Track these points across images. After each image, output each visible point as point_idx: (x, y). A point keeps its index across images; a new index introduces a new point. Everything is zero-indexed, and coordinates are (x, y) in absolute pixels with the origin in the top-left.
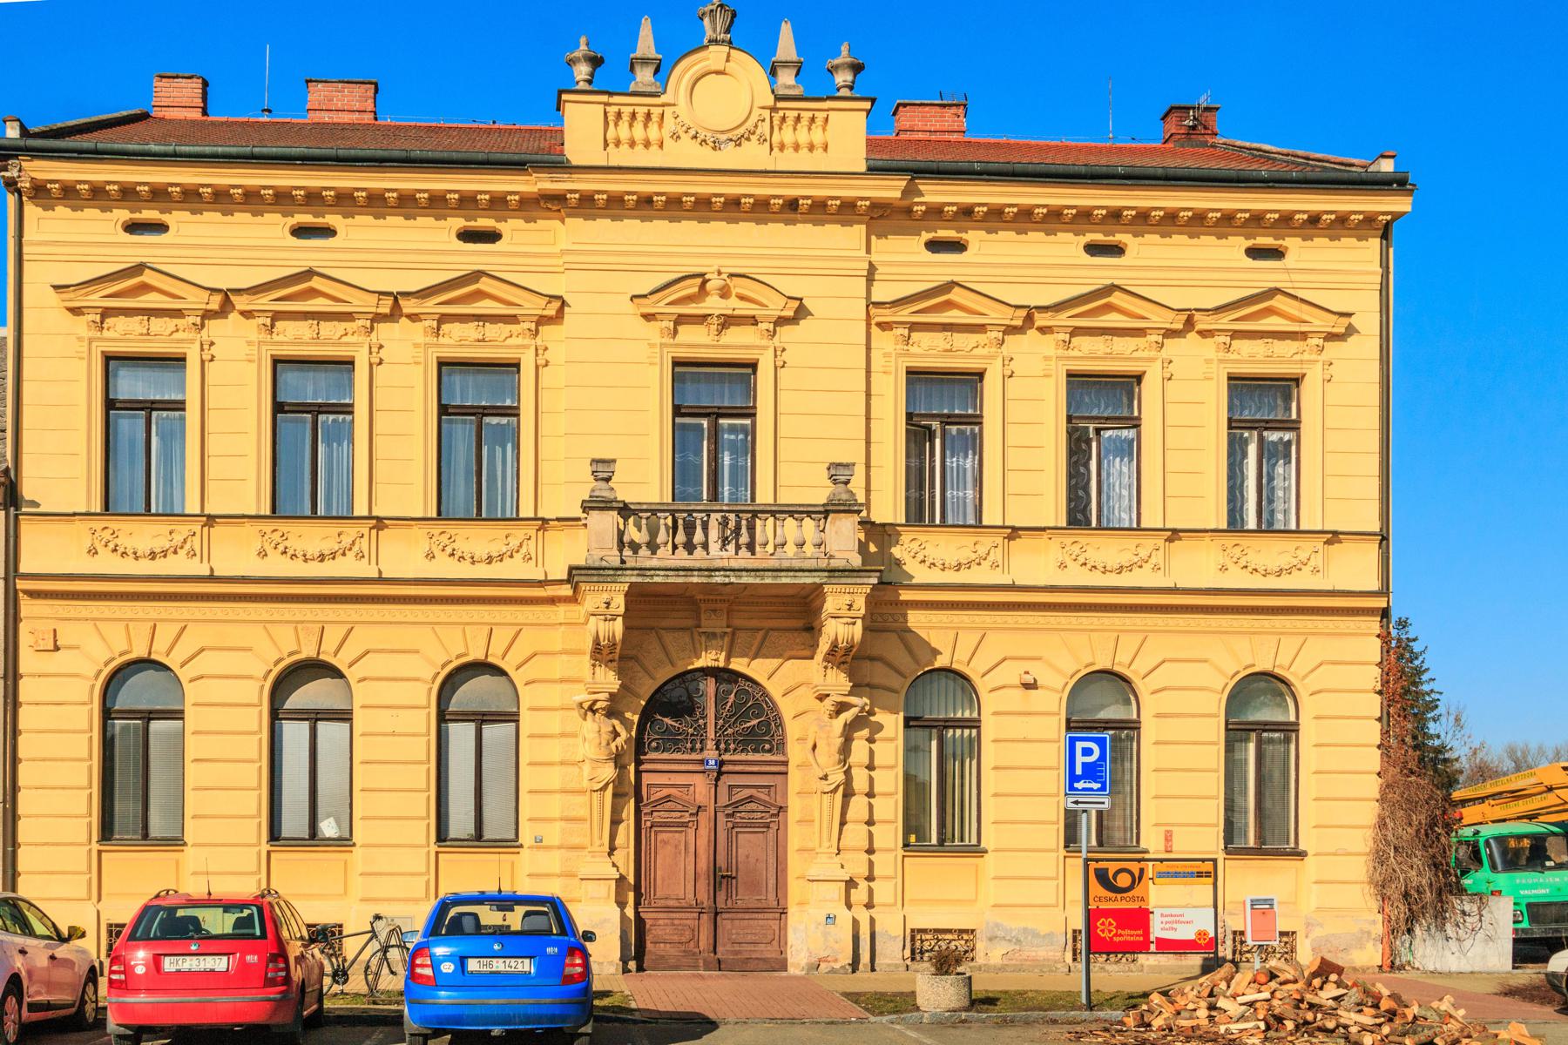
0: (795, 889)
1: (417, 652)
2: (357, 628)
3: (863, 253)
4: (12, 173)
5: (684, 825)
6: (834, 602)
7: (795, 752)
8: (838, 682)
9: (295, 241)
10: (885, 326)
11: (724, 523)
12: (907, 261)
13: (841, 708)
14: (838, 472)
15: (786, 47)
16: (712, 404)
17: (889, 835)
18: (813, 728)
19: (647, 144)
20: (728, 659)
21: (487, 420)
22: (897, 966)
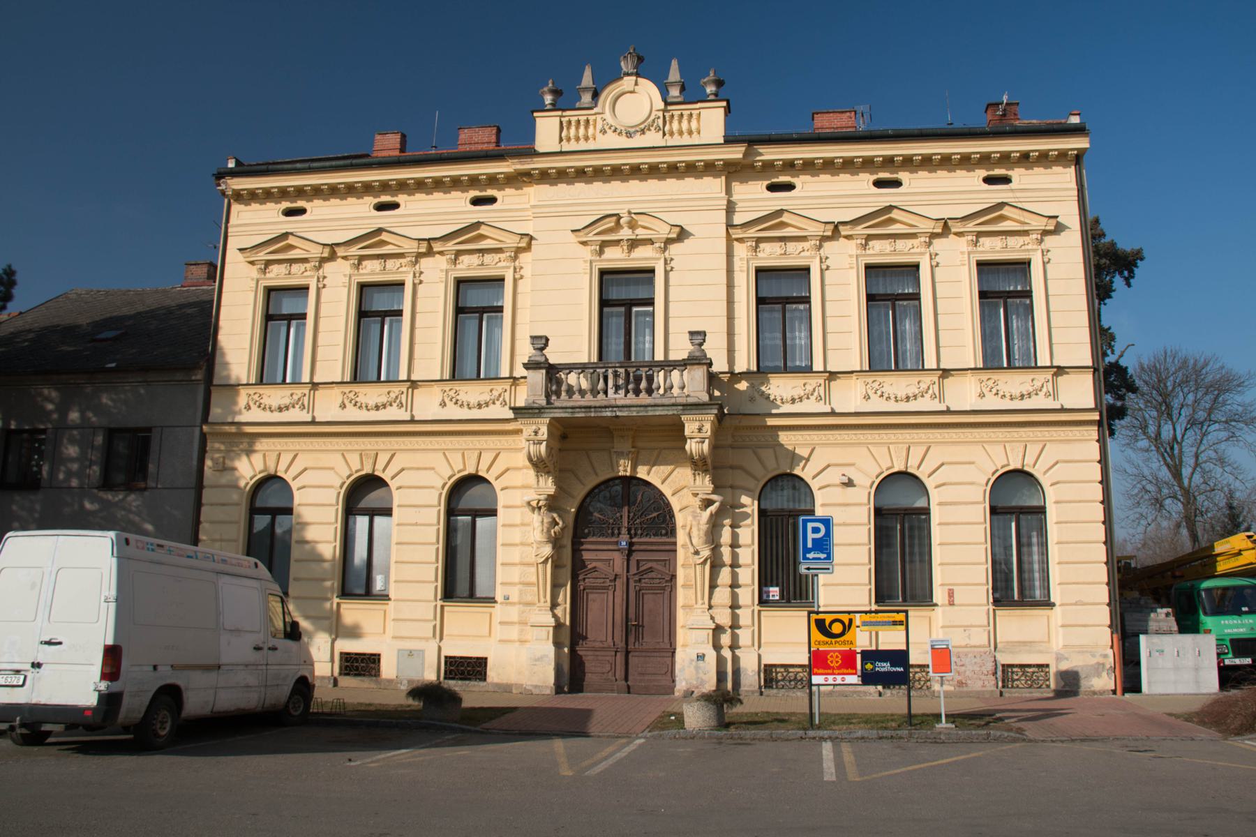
0: (681, 636)
1: (433, 469)
2: (1048, 445)
3: (723, 194)
4: (223, 187)
5: (606, 588)
6: (690, 428)
7: (681, 537)
8: (704, 484)
9: (986, 187)
10: (740, 240)
11: (616, 375)
12: (753, 197)
13: (707, 503)
14: (698, 336)
15: (674, 75)
16: (623, 297)
17: (747, 595)
18: (690, 518)
19: (690, 133)
20: (634, 468)
21: (635, 309)
22: (753, 692)
